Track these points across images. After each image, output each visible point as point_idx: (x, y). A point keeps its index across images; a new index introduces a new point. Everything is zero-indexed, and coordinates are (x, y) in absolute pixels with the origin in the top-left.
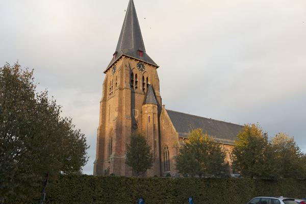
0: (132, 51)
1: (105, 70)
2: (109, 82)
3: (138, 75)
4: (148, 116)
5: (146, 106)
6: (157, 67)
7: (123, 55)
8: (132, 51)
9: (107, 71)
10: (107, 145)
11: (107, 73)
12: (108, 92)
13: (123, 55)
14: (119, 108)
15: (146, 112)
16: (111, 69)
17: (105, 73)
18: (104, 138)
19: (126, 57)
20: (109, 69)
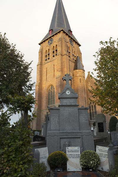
0: (60, 25)
1: (40, 42)
2: (44, 51)
3: (70, 48)
4: (80, 78)
5: (77, 71)
6: (80, 46)
7: (62, 30)
8: (60, 25)
9: (42, 43)
10: (45, 98)
11: (41, 45)
12: (44, 58)
13: (62, 30)
14: (61, 69)
15: (78, 75)
16: (47, 42)
17: (40, 44)
18: (41, 93)
19: (64, 32)
20: (44, 41)
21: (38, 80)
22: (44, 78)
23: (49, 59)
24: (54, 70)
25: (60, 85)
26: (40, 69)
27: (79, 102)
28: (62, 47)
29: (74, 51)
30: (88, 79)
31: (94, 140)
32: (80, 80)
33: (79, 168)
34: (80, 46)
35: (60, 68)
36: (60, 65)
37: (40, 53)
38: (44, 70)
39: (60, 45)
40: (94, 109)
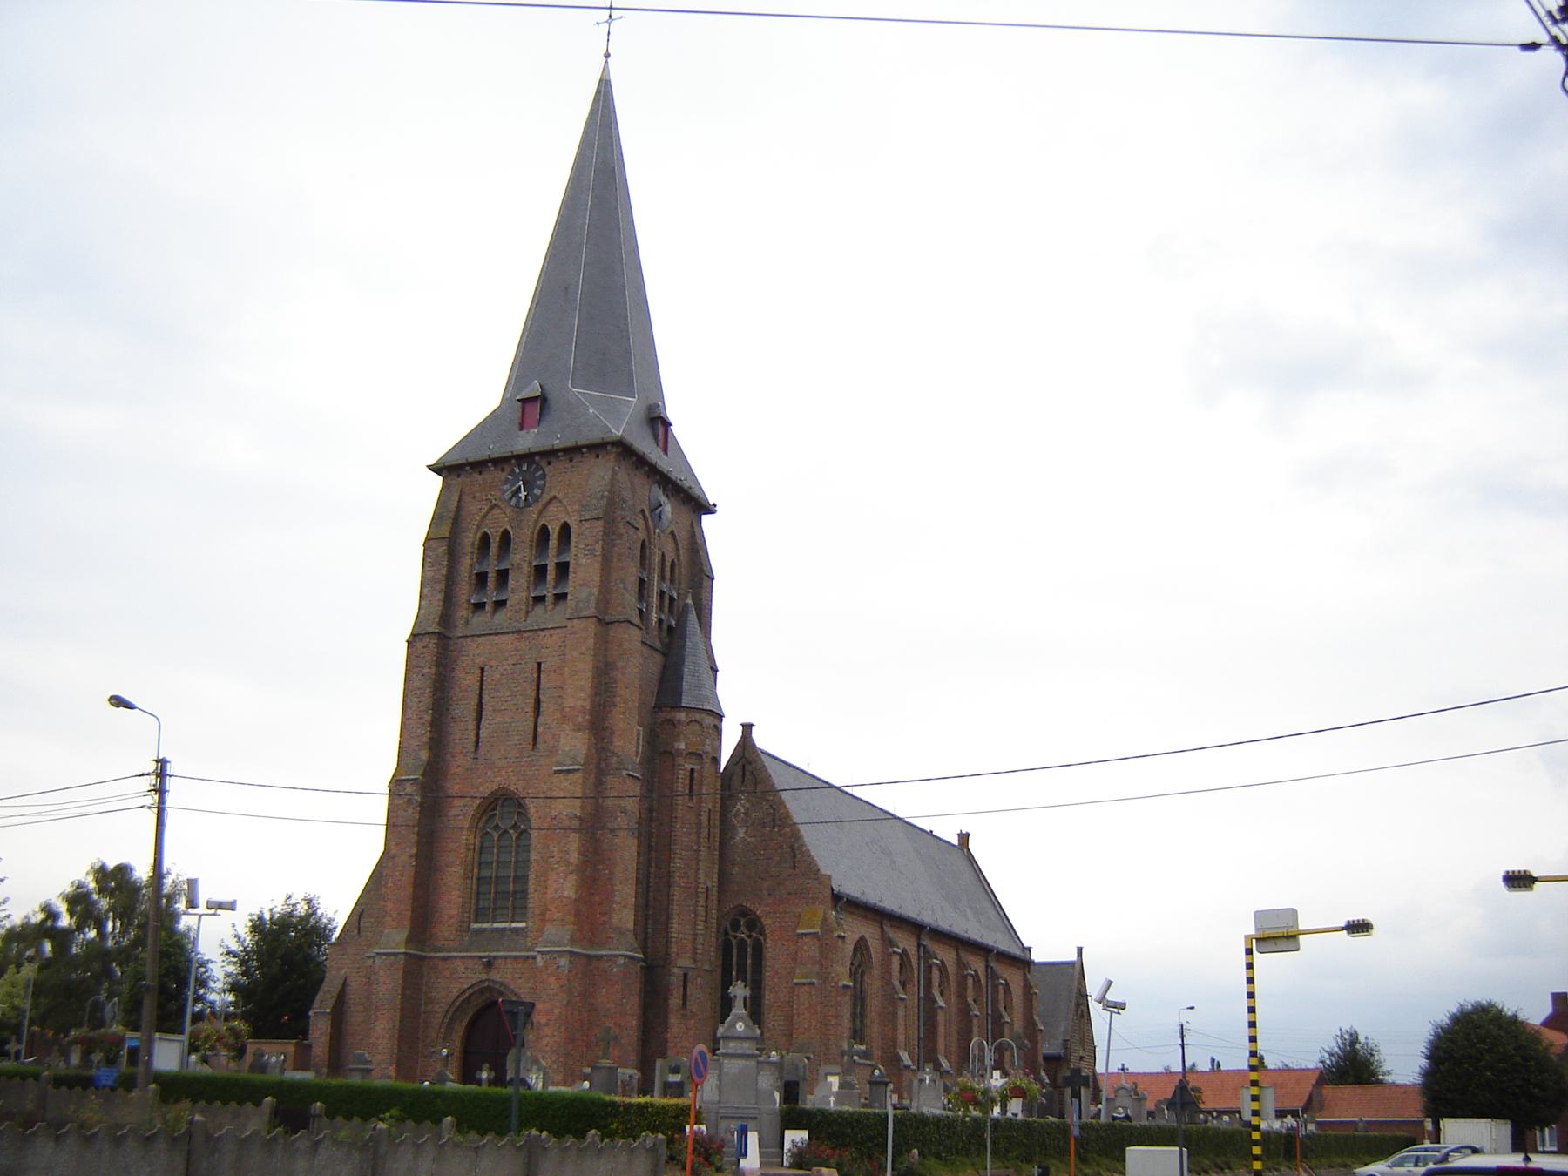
2: (470, 539)
4: (688, 766)
6: (710, 509)
15: (682, 746)
21: (415, 743)
22: (461, 731)
23: (500, 604)
24: (538, 702)
25: (580, 819)
26: (437, 664)
27: (668, 918)
28: (606, 560)
29: (668, 564)
30: (739, 771)
31: (519, 911)
32: (691, 780)
33: (750, 1134)
34: (710, 509)
35: (587, 705)
36: (588, 690)
37: (442, 549)
38: (465, 680)
39: (598, 546)
40: (753, 964)
